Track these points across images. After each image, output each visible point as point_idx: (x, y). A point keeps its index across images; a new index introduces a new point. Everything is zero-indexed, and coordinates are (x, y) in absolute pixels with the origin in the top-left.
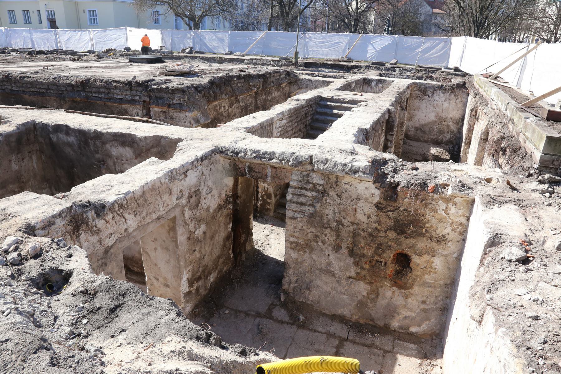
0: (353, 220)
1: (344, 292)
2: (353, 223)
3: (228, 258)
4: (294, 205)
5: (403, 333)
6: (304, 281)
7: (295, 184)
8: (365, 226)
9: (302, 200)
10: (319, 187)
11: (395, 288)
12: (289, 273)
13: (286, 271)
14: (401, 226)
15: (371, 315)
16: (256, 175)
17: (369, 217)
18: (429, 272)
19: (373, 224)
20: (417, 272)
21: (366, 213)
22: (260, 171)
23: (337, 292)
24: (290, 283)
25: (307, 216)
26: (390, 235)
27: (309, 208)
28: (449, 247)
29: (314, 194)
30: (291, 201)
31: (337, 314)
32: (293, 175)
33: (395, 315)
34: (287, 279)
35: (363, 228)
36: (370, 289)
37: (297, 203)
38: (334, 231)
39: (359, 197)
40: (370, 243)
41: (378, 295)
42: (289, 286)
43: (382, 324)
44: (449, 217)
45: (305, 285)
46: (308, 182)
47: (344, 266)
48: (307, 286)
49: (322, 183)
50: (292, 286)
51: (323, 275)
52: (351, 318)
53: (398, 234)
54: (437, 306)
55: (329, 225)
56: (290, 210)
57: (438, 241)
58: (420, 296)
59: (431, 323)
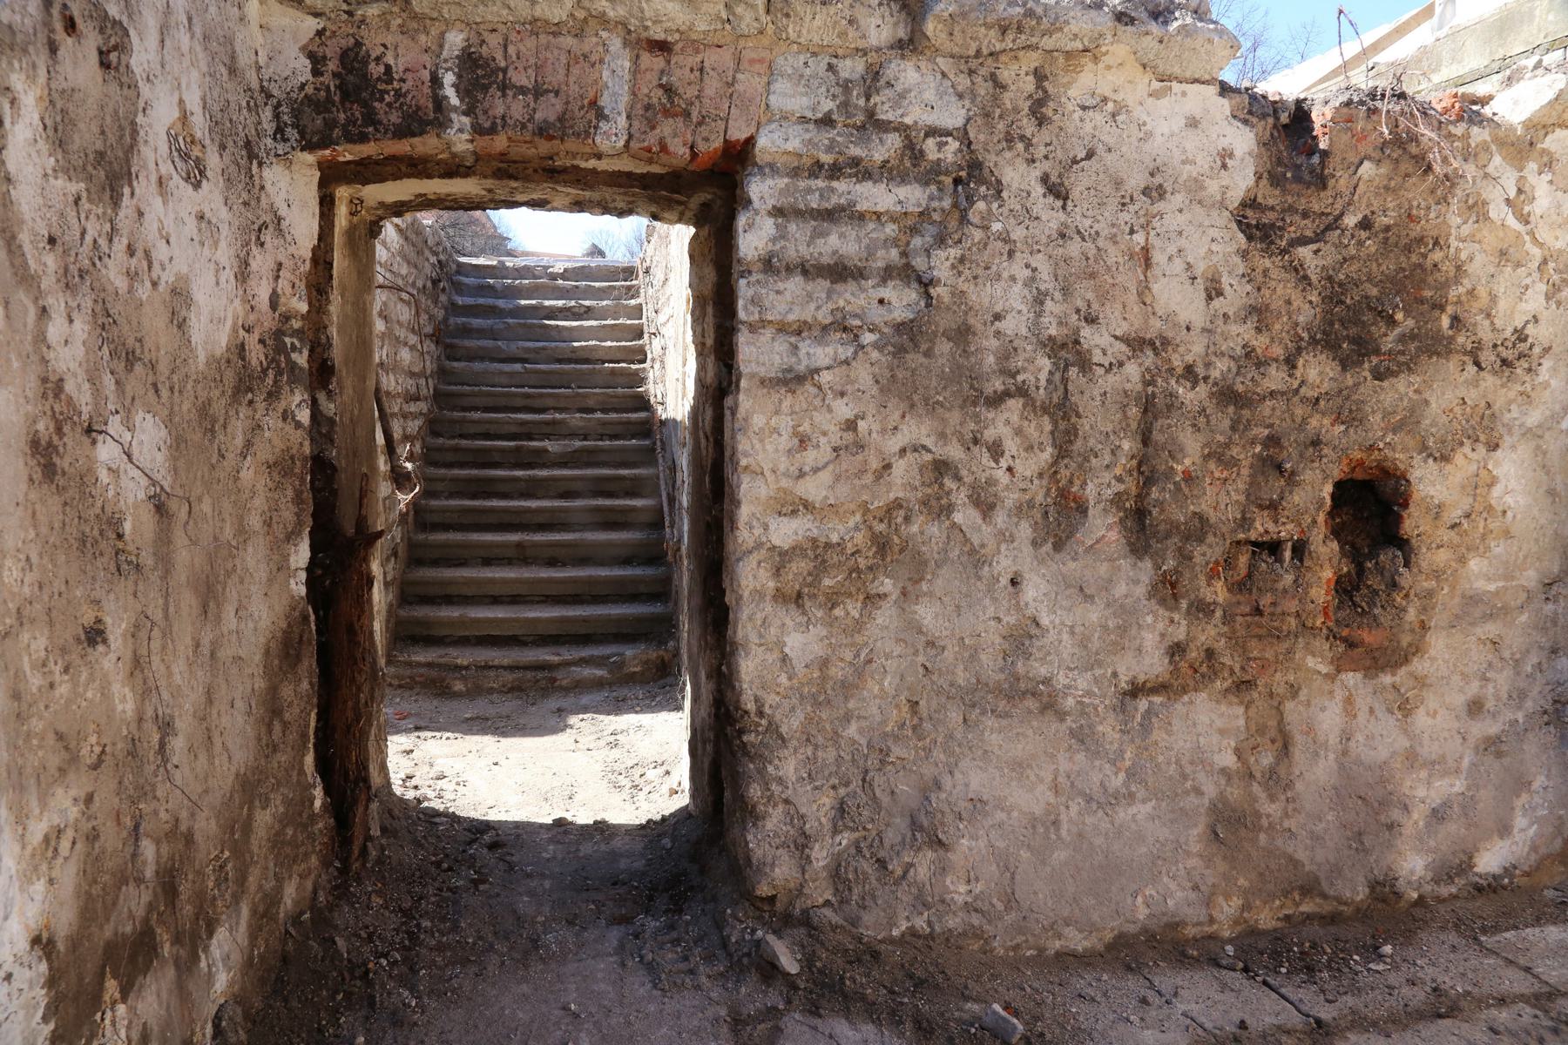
0: (1137, 323)
1: (1126, 784)
2: (1137, 344)
3: (298, 811)
4: (794, 285)
5: (1455, 897)
6: (885, 799)
7: (794, 144)
8: (1195, 349)
9: (840, 243)
10: (941, 145)
11: (1351, 678)
12: (780, 781)
13: (762, 771)
14: (1353, 317)
15: (1294, 862)
16: (517, 108)
17: (1214, 291)
18: (1484, 537)
19: (1234, 329)
20: (1432, 557)
21: (1200, 268)
22: (555, 78)
23: (1089, 800)
24: (801, 844)
25: (875, 345)
26: (1312, 374)
27: (887, 292)
28: (1546, 385)
29: (912, 196)
30: (768, 264)
31: (1132, 929)
32: (780, 86)
33: (1396, 814)
34: (775, 820)
35: (1189, 359)
36: (1242, 722)
37: (807, 270)
38: (1045, 410)
39: (1158, 180)
40: (1227, 446)
41: (1285, 746)
42: (805, 861)
43: (1361, 893)
44: (1532, 233)
45: (901, 823)
46: (873, 124)
47: (1105, 628)
48: (915, 825)
49: (959, 122)
50: (820, 856)
51: (990, 722)
52: (1212, 920)
53: (1345, 365)
54: (1529, 704)
55: (1013, 376)
56: (764, 323)
57: (1504, 362)
58: (1456, 678)
59: (1537, 799)
